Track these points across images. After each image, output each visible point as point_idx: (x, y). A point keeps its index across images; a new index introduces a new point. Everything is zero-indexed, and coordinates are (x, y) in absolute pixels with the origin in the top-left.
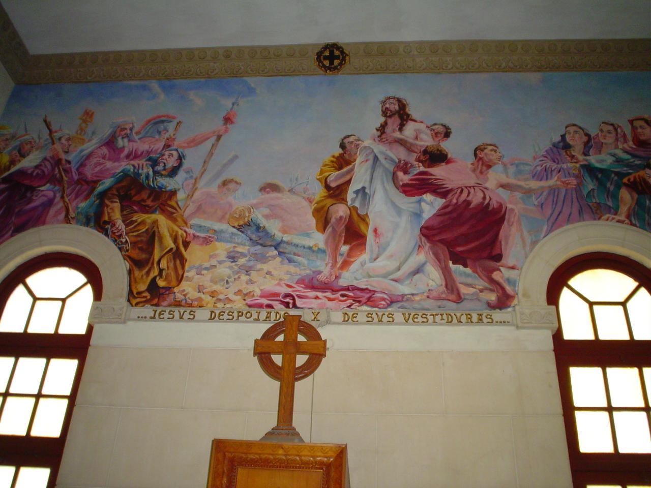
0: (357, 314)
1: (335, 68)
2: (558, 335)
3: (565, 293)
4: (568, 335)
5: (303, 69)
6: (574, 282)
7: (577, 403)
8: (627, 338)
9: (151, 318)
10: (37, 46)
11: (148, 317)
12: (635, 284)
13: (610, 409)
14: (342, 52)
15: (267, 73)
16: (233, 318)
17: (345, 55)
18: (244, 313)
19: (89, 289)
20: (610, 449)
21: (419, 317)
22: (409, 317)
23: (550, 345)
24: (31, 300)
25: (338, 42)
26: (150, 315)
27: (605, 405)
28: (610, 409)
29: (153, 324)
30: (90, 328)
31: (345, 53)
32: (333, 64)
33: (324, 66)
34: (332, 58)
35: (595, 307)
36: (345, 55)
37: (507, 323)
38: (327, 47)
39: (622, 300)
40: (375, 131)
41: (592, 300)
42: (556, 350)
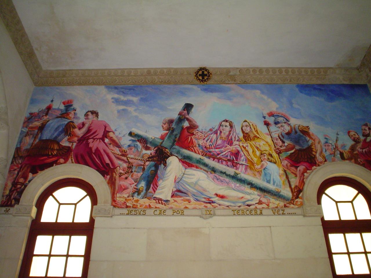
0: (166, 211)
1: (205, 81)
2: (322, 219)
3: (324, 198)
4: (326, 218)
5: (109, 82)
6: (327, 191)
7: (333, 250)
8: (354, 219)
9: (127, 214)
10: (46, 66)
11: (125, 214)
12: (356, 192)
13: (348, 253)
14: (208, 73)
15: (223, 82)
16: (179, 213)
17: (210, 74)
18: (176, 211)
19: (88, 200)
20: (350, 273)
21: (133, 211)
22: (275, 212)
23: (320, 223)
24: (58, 205)
25: (206, 67)
26: (126, 213)
27: (346, 251)
28: (348, 253)
29: (128, 217)
30: (92, 220)
31: (210, 73)
32: (204, 78)
33: (199, 79)
34: (203, 75)
35: (338, 204)
36: (210, 74)
37: (292, 214)
38: (201, 69)
39: (351, 200)
40: (29, 114)
41: (337, 200)
42: (323, 225)
